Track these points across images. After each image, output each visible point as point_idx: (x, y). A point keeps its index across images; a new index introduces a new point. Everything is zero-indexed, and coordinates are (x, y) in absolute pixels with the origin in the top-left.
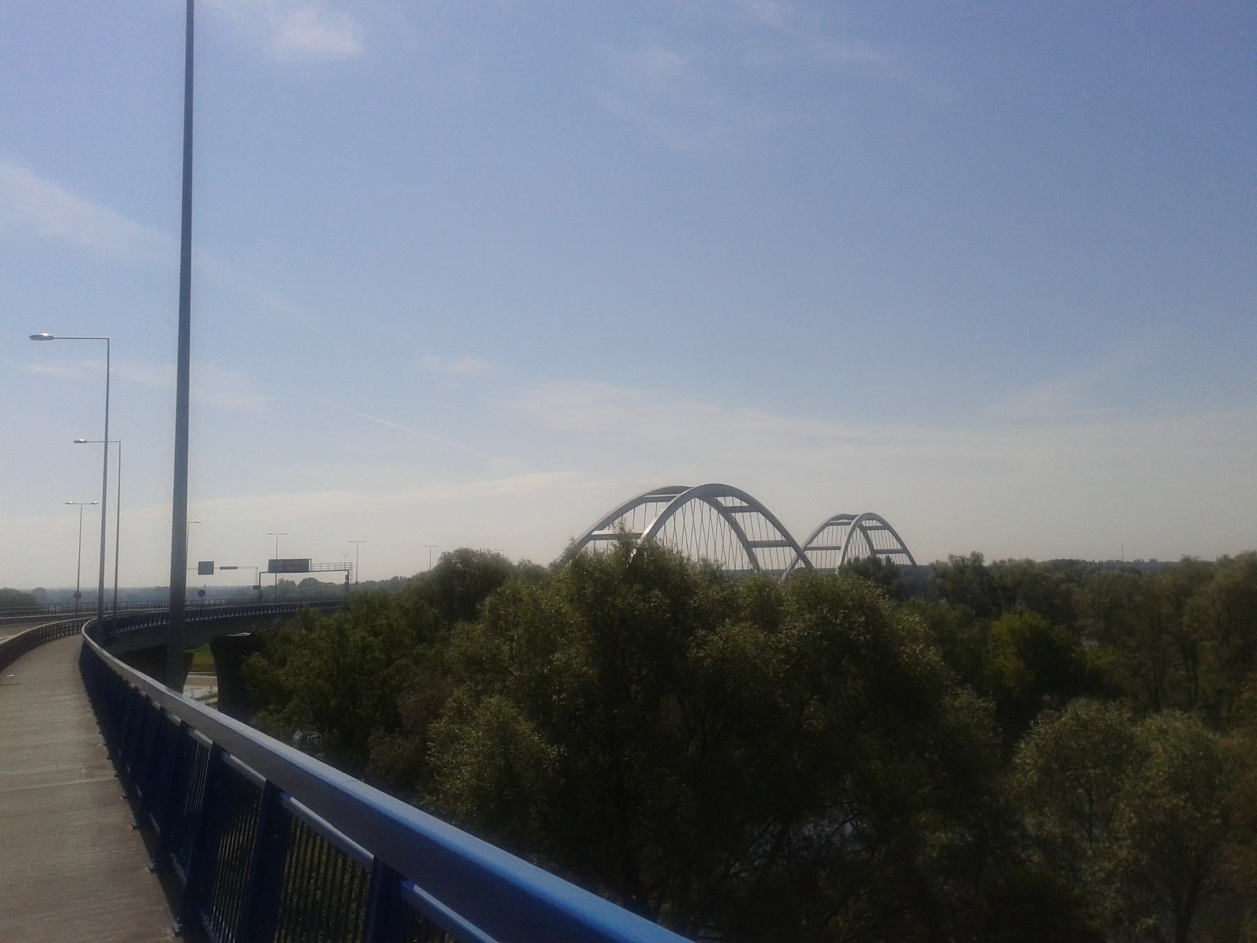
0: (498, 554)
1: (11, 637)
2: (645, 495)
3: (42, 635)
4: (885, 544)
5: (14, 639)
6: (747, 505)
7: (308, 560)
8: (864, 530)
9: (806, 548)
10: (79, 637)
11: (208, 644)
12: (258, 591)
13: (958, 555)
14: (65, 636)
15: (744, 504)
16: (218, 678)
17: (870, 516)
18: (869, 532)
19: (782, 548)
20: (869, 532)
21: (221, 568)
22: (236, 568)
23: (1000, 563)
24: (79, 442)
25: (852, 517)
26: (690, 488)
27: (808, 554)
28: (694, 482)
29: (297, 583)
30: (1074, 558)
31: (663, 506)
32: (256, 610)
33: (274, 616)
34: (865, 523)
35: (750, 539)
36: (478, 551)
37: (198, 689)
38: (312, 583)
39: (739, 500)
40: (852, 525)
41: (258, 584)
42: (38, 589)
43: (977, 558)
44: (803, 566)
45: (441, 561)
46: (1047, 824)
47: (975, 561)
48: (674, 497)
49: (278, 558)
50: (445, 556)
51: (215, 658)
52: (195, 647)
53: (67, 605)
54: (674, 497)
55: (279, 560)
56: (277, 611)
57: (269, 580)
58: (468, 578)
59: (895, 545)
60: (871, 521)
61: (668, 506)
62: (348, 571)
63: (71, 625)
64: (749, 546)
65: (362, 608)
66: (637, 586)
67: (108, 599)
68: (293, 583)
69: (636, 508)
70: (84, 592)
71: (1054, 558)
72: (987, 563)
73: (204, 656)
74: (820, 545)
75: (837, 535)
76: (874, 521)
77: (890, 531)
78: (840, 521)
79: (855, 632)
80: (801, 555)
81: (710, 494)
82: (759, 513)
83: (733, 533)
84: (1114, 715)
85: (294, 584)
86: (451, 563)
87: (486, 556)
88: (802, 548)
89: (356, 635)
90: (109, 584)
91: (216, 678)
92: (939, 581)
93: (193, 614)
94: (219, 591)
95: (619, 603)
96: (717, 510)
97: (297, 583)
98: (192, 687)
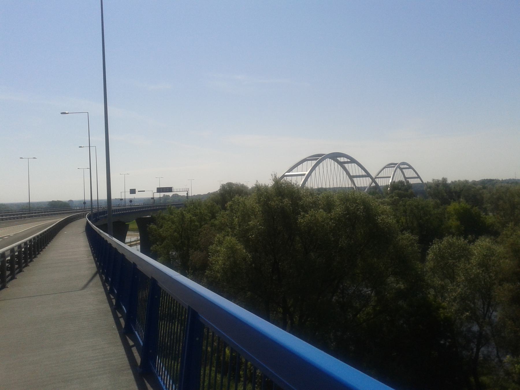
0: (452, 182)
1: (63, 219)
2: (308, 158)
3: (73, 218)
4: (410, 175)
5: (63, 220)
6: (350, 161)
7: (172, 187)
8: (401, 169)
9: (376, 178)
10: (85, 219)
11: (135, 220)
12: (153, 200)
13: (436, 179)
14: (81, 218)
15: (349, 160)
16: (140, 234)
18: (403, 170)
19: (362, 178)
20: (403, 170)
21: (139, 191)
22: (144, 191)
23: (454, 182)
24: (81, 147)
25: (396, 164)
26: (325, 154)
27: (377, 180)
28: (327, 152)
29: (171, 196)
30: (491, 178)
31: (314, 162)
32: (139, 209)
33: (158, 209)
34: (402, 166)
35: (352, 174)
36: (235, 183)
37: (133, 237)
38: (176, 196)
39: (346, 159)
40: (396, 167)
41: (153, 197)
42: (230, 183)
43: (444, 180)
44: (375, 185)
45: (221, 187)
47: (443, 181)
48: (318, 159)
49: (160, 187)
50: (222, 185)
51: (138, 226)
52: (129, 222)
54: (319, 158)
55: (350, 163)
56: (161, 207)
57: (158, 195)
58: (232, 194)
59: (415, 175)
60: (404, 166)
61: (316, 162)
62: (188, 191)
63: (83, 215)
64: (351, 177)
65: (191, 206)
66: (280, 198)
67: (95, 205)
68: (169, 196)
70: (87, 201)
71: (483, 179)
72: (449, 181)
73: (133, 225)
74: (382, 176)
76: (405, 165)
77: (413, 170)
78: (391, 166)
79: (359, 212)
80: (373, 180)
81: (334, 156)
82: (355, 164)
83: (345, 172)
84: (204, 226)
85: (170, 196)
86: (225, 188)
87: (238, 186)
88: (374, 178)
89: (188, 216)
90: (95, 198)
91: (139, 233)
92: (428, 190)
93: (116, 211)
94: (140, 200)
95: (273, 203)
97: (171, 196)
98: (131, 237)
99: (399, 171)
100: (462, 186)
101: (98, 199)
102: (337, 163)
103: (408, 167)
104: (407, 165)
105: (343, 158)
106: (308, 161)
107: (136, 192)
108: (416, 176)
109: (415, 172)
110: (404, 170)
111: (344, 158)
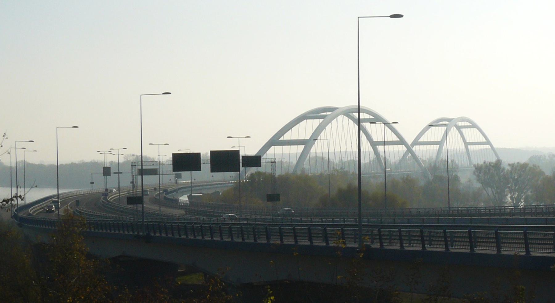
8: (459, 128)
17: (463, 120)
20: (461, 129)
34: (460, 124)
46: (108, 192)
53: (112, 224)
64: (467, 144)
69: (300, 123)
75: (436, 134)
76: (466, 122)
77: (478, 129)
96: (353, 121)
99: (454, 130)
100: (409, 178)
101: (11, 188)
102: (347, 117)
103: (471, 125)
104: (467, 122)
105: (363, 113)
106: (307, 120)
107: (111, 174)
108: (484, 140)
109: (460, 134)
110: (463, 130)
111: (364, 114)
